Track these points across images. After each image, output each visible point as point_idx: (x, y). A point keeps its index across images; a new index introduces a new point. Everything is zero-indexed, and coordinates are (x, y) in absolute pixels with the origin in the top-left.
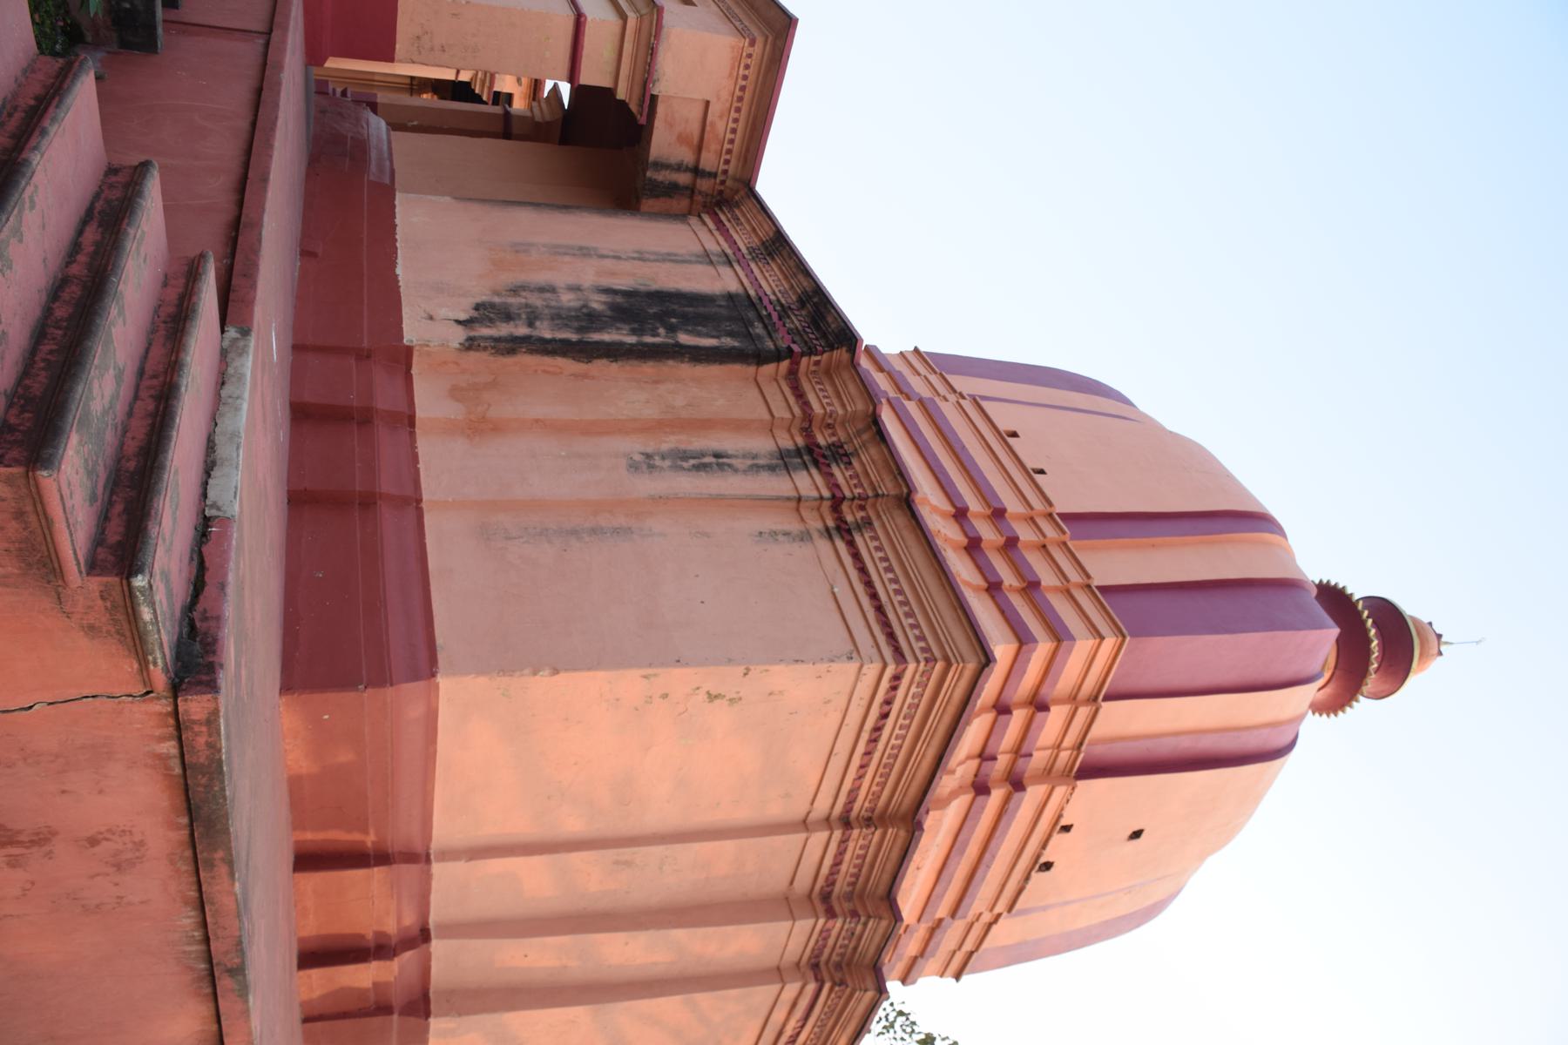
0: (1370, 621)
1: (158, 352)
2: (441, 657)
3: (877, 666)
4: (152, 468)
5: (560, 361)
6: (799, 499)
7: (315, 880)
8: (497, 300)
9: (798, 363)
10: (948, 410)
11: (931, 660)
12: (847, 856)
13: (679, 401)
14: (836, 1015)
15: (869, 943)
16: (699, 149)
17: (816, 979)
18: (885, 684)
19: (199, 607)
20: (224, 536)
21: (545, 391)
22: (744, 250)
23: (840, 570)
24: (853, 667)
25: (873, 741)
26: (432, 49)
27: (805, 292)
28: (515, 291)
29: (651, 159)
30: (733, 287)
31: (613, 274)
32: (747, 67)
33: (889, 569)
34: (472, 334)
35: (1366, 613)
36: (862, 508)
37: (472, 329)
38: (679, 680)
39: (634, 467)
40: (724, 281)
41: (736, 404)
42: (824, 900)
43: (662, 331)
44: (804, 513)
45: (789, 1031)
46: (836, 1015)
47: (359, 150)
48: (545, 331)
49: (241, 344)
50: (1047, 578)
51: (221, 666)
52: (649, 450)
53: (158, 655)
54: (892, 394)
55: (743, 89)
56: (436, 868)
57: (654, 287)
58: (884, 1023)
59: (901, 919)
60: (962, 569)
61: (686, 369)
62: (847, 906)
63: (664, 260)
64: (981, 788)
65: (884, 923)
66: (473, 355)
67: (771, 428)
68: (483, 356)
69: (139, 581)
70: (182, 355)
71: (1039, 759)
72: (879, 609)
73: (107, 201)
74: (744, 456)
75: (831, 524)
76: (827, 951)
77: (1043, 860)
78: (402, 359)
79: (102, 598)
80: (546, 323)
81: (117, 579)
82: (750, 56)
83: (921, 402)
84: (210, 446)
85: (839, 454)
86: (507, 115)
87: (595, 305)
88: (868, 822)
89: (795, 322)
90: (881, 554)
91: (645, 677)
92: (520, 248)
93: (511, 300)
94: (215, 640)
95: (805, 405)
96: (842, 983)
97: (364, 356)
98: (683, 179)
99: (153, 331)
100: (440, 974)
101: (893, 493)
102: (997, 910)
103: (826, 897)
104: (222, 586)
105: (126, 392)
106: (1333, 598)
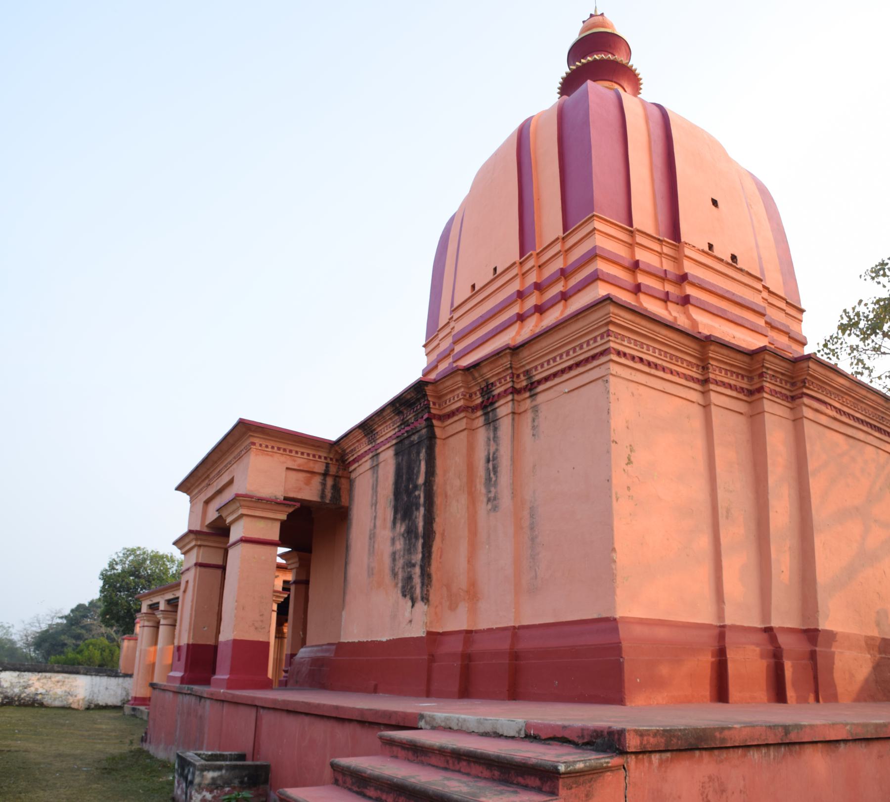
0: (583, 61)
1: (434, 760)
2: (604, 615)
3: (611, 365)
4: (498, 762)
5: (435, 549)
6: (513, 413)
7: (734, 691)
8: (400, 585)
9: (435, 415)
10: (459, 326)
12: (726, 380)
13: (457, 483)
14: (823, 385)
16: (313, 473)
17: (801, 397)
18: (622, 360)
19: (576, 740)
20: (536, 727)
21: (451, 556)
22: (370, 446)
23: (555, 388)
24: (612, 379)
25: (656, 366)
26: (262, 621)
27: (393, 411)
28: (395, 575)
29: (318, 500)
30: (391, 453)
31: (385, 520)
33: (554, 359)
34: (419, 598)
35: (578, 63)
36: (518, 376)
37: (417, 598)
38: (619, 479)
39: (495, 508)
40: (388, 458)
41: (458, 450)
42: (753, 394)
43: (417, 493)
44: (522, 410)
45: (833, 413)
46: (823, 385)
47: (317, 663)
48: (418, 557)
49: (428, 719)
50: (558, 264)
51: (610, 727)
52: (485, 500)
53: (603, 761)
54: (450, 360)
55: (279, 449)
56: (728, 622)
57: (391, 496)
58: (831, 356)
59: (765, 346)
60: (553, 316)
61: (439, 479)
62: (756, 379)
63: (376, 492)
64: (685, 301)
65: (767, 357)
66: (431, 598)
67: (472, 430)
68: (432, 591)
69: (562, 768)
70: (435, 747)
71: (668, 265)
72: (578, 365)
73: (353, 784)
74: (489, 445)
75: (527, 394)
76: (784, 391)
77: (730, 261)
78: (433, 637)
79: (571, 788)
80: (413, 557)
81: (561, 780)
82: (261, 445)
83: (455, 342)
84: (485, 735)
85: (487, 390)
86: (295, 582)
87: (403, 530)
88: (705, 368)
89: (410, 417)
90: (545, 364)
91: (617, 500)
92: (371, 572)
93: (400, 576)
94: (595, 731)
95: (458, 410)
96: (804, 382)
97: (432, 658)
98: (330, 482)
99: (422, 763)
100: (793, 623)
101: (509, 358)
102: (761, 288)
103: (751, 393)
104: (564, 727)
105: (456, 776)
106: (569, 85)
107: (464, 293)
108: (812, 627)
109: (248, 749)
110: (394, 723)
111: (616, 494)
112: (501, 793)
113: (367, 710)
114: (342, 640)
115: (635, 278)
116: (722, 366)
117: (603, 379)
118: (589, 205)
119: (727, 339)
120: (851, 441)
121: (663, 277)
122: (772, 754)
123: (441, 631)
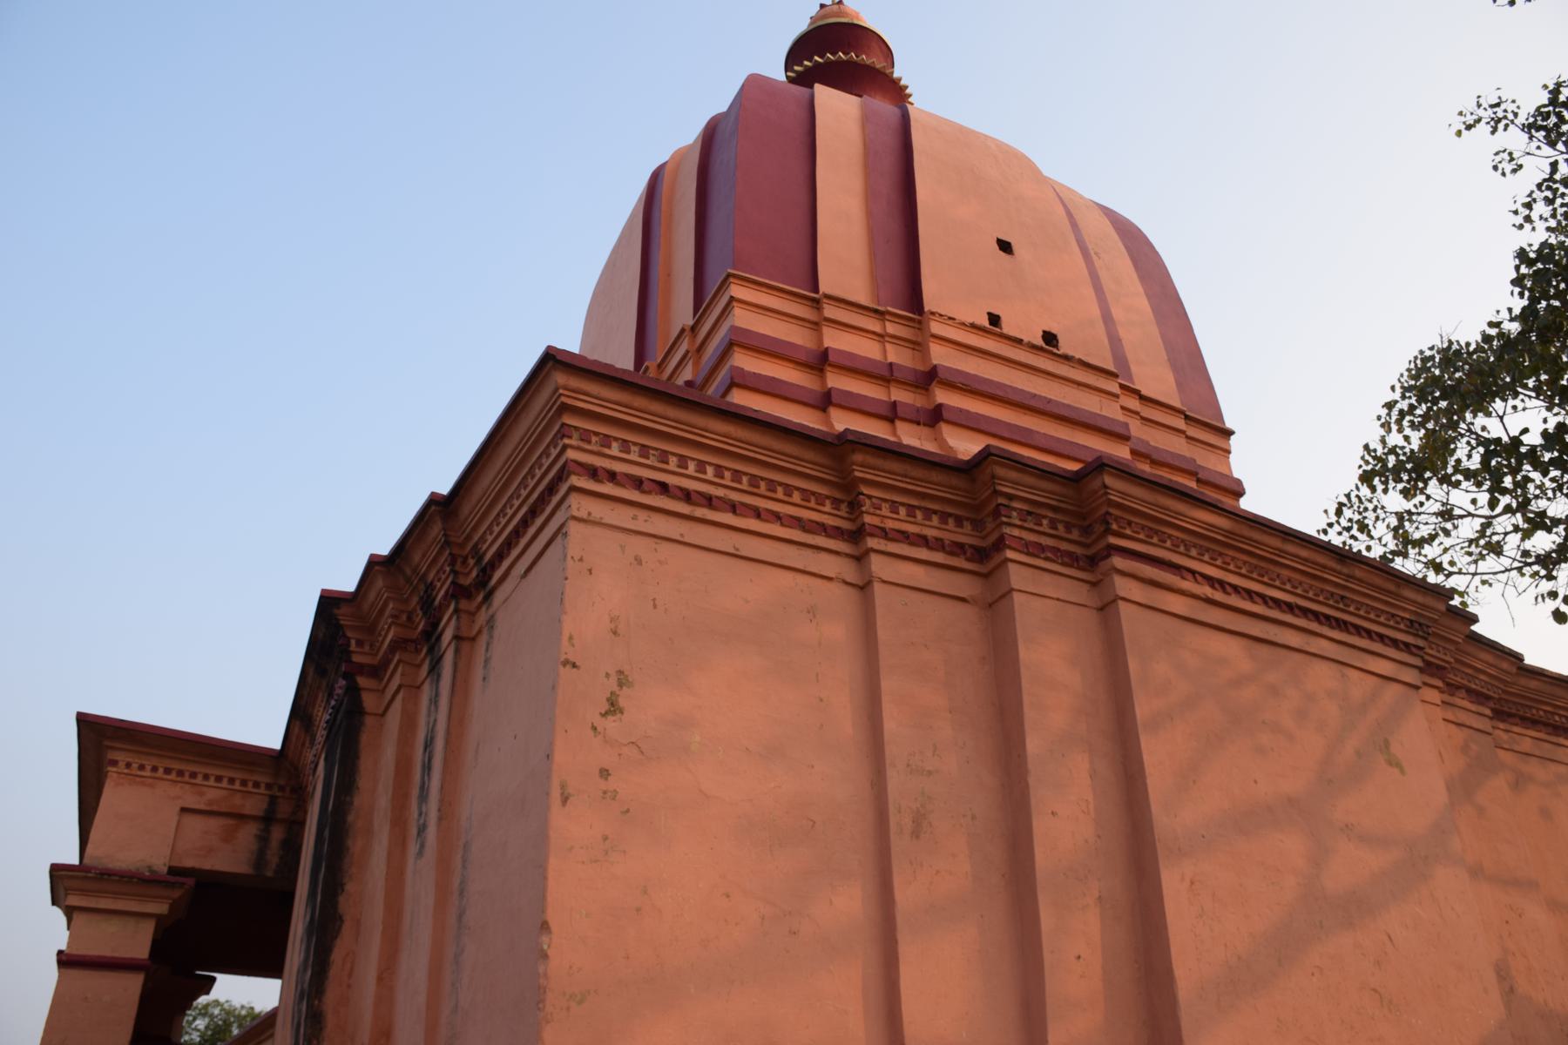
3: (574, 499)
9: (361, 666)
11: (565, 431)
15: (1044, 492)
16: (241, 817)
17: (1108, 556)
32: (142, 767)
38: (573, 756)
42: (984, 557)
55: (168, 771)
62: (990, 526)
71: (896, 355)
76: (1064, 546)
82: (128, 765)
88: (854, 506)
91: (565, 800)
98: (277, 834)
102: (1115, 388)
103: (981, 555)
111: (563, 786)
120: (1265, 651)
121: (886, 375)
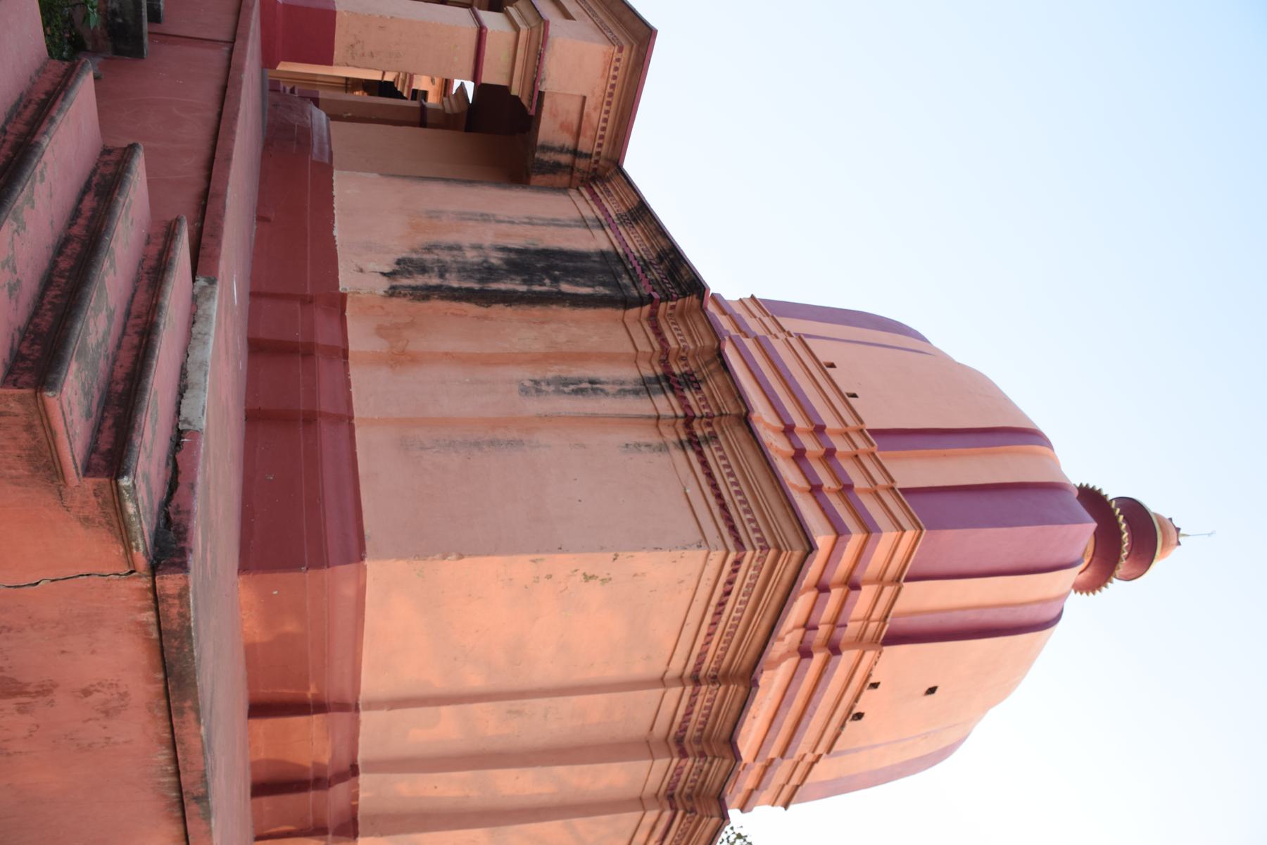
0: (1121, 517)
1: (142, 297)
2: (368, 544)
3: (721, 553)
4: (136, 390)
5: (466, 306)
6: (658, 418)
8: (414, 256)
9: (657, 308)
10: (779, 346)
11: (765, 548)
12: (697, 708)
13: (561, 338)
16: (578, 134)
17: (671, 808)
18: (728, 568)
19: (174, 503)
20: (194, 446)
21: (453, 329)
22: (614, 217)
23: (692, 475)
25: (718, 613)
26: (363, 55)
28: (429, 249)
30: (605, 246)
31: (508, 235)
32: (616, 69)
33: (731, 474)
34: (395, 283)
35: (1118, 511)
36: (709, 425)
37: (394, 280)
38: (562, 563)
39: (525, 391)
40: (598, 241)
41: (608, 340)
42: (678, 743)
43: (547, 281)
47: (304, 136)
48: (453, 282)
49: (209, 290)
50: (859, 482)
51: (191, 551)
52: (537, 377)
53: (140, 541)
54: (733, 332)
55: (613, 86)
56: (364, 715)
57: (541, 246)
60: (790, 474)
61: (566, 312)
62: (697, 748)
63: (549, 225)
64: (805, 652)
65: (726, 762)
66: (395, 301)
67: (635, 360)
68: (403, 301)
69: (125, 482)
70: (161, 299)
71: (852, 628)
72: (723, 506)
73: (103, 176)
74: (614, 383)
75: (684, 437)
76: (680, 785)
77: (855, 711)
78: (338, 303)
79: (96, 495)
81: (107, 480)
84: (183, 373)
85: (691, 381)
86: (423, 108)
87: (494, 261)
88: (714, 679)
89: (655, 274)
91: (534, 561)
92: (433, 215)
93: (427, 257)
94: (186, 530)
95: (663, 341)
96: (693, 810)
97: (307, 301)
98: (565, 159)
99: (138, 280)
102: (818, 752)
103: (679, 741)
104: (192, 486)
105: (116, 329)
106: (1091, 498)
107: (824, 352)
108: (360, 828)
109: (167, 26)
110: (203, 241)
112: (87, 394)
113: (224, 203)
114: (336, 173)
115: (838, 585)
116: (716, 703)
117: (703, 542)
118: (935, 523)
119: (752, 708)
121: (837, 623)
122: (167, 780)
123: (347, 314)
